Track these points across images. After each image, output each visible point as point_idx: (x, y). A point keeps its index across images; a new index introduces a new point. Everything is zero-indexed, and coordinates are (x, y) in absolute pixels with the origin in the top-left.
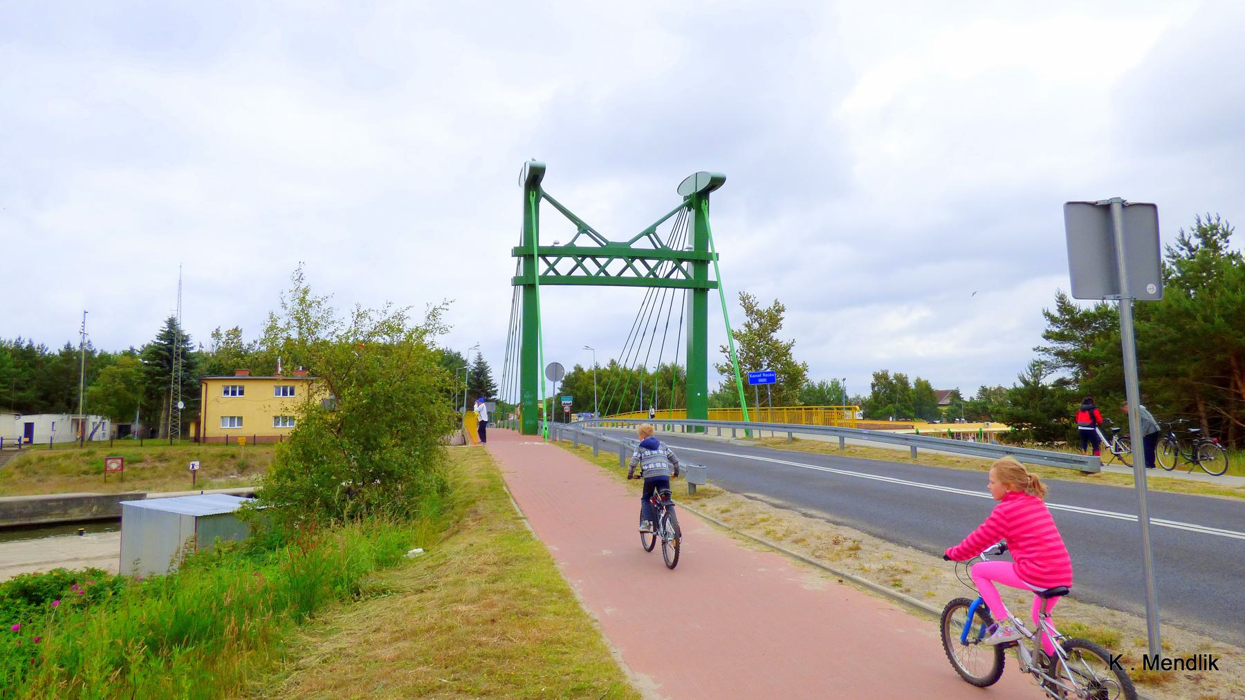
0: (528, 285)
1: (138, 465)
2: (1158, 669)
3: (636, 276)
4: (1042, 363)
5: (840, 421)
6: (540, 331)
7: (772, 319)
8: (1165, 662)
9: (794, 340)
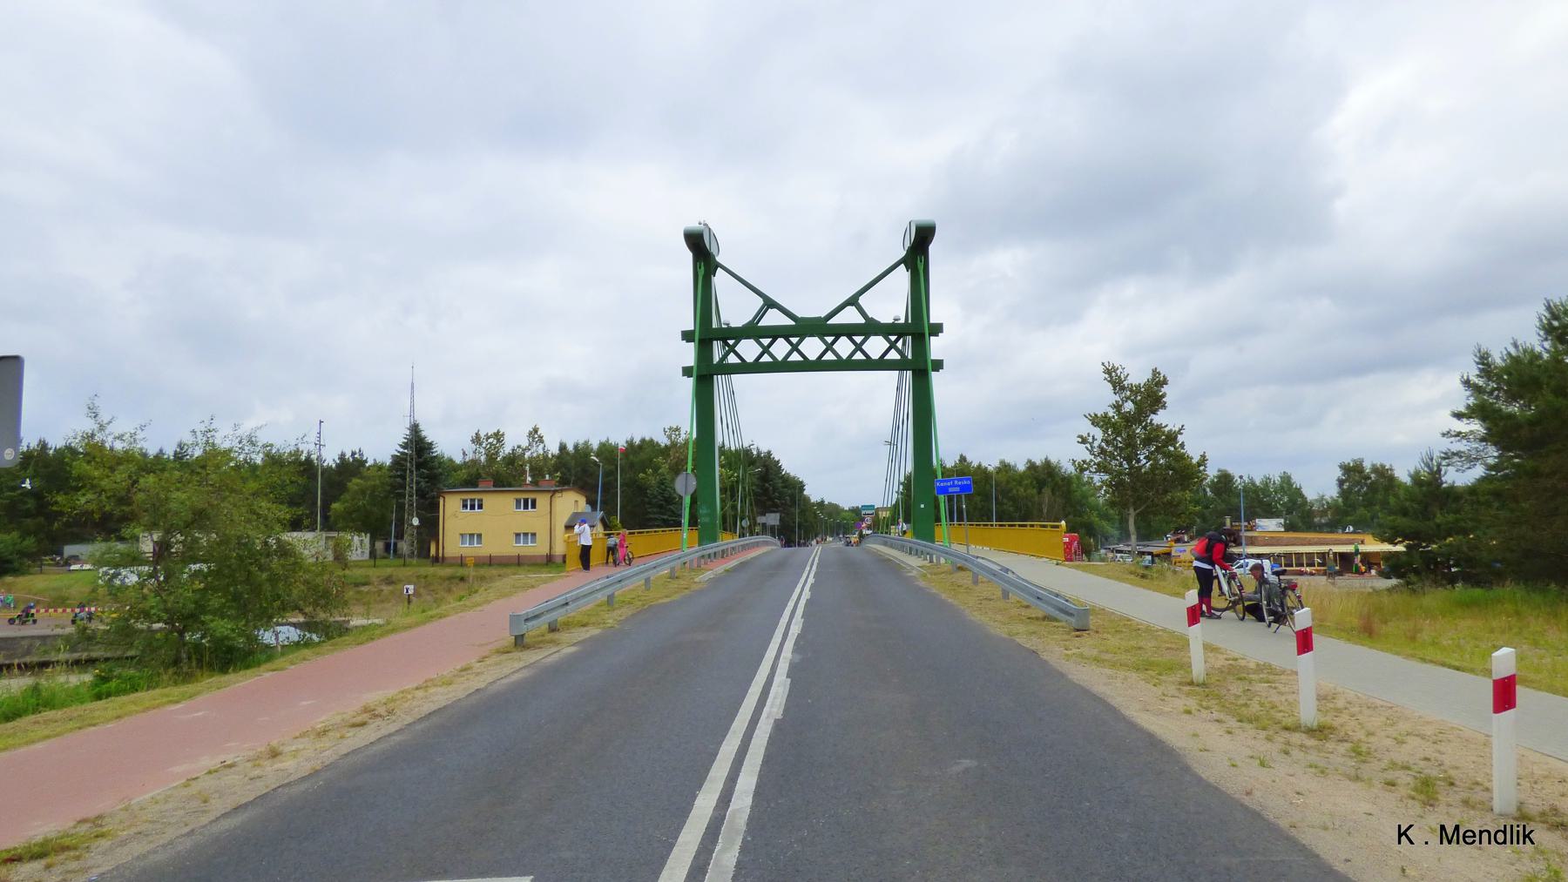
0: (705, 376)
1: (365, 589)
2: (1458, 843)
3: (835, 358)
4: (1454, 454)
5: (1249, 534)
6: (934, 419)
7: (1151, 396)
8: (1467, 835)
9: (1183, 426)
